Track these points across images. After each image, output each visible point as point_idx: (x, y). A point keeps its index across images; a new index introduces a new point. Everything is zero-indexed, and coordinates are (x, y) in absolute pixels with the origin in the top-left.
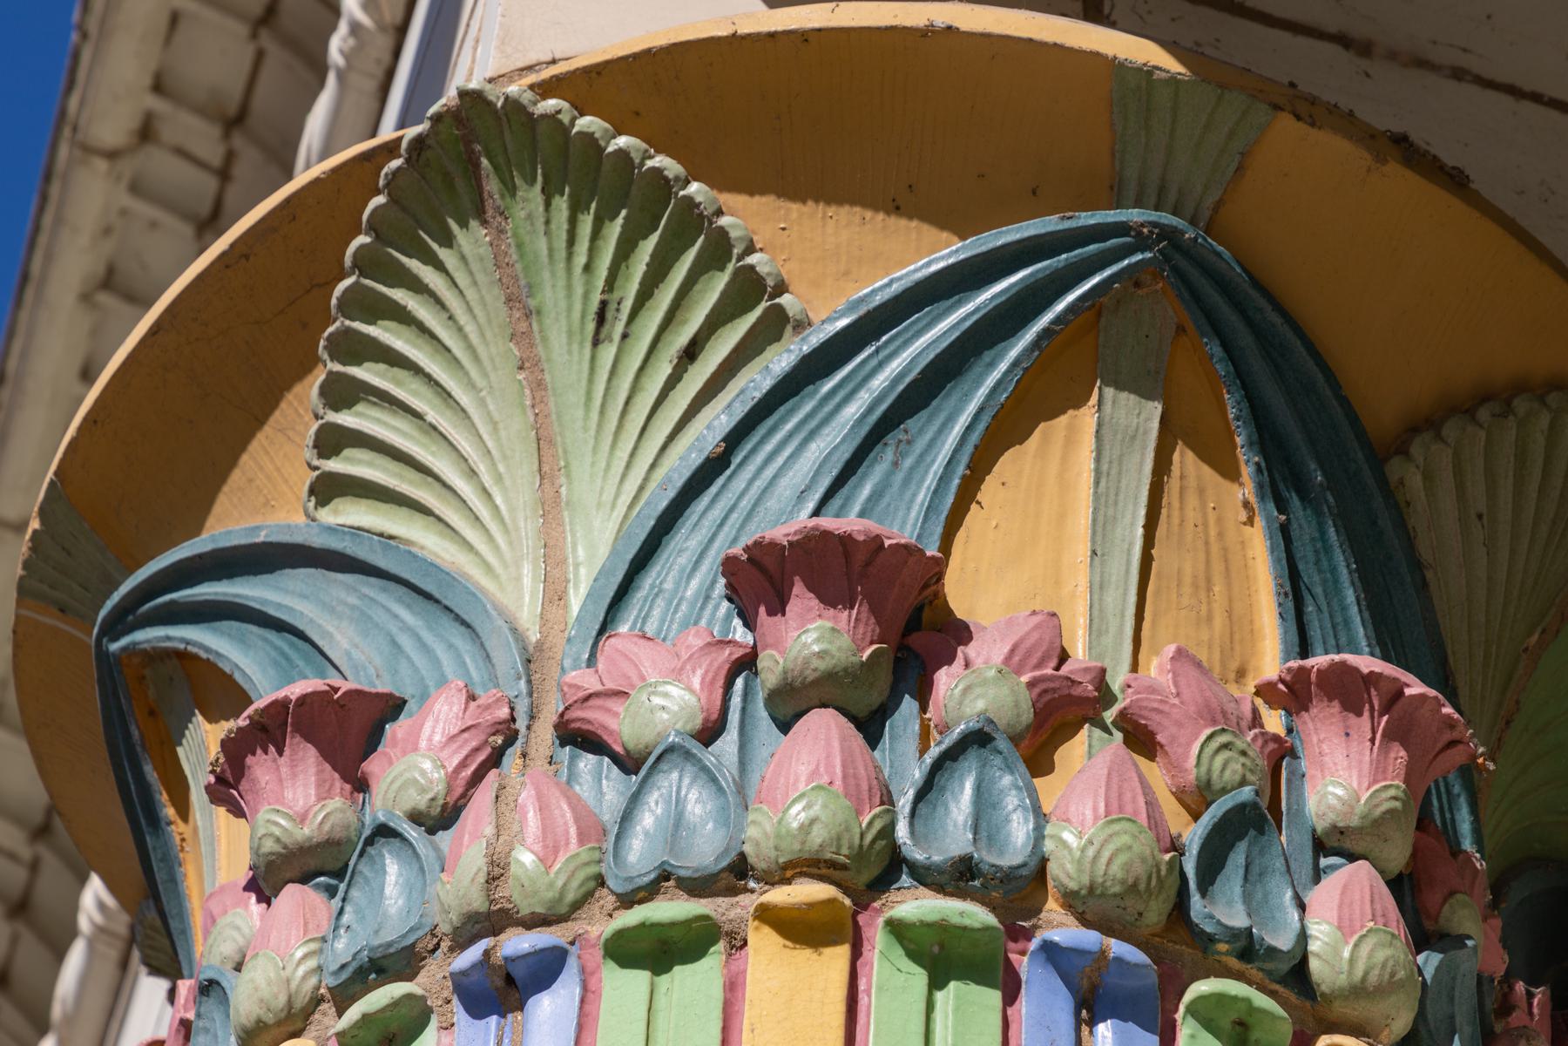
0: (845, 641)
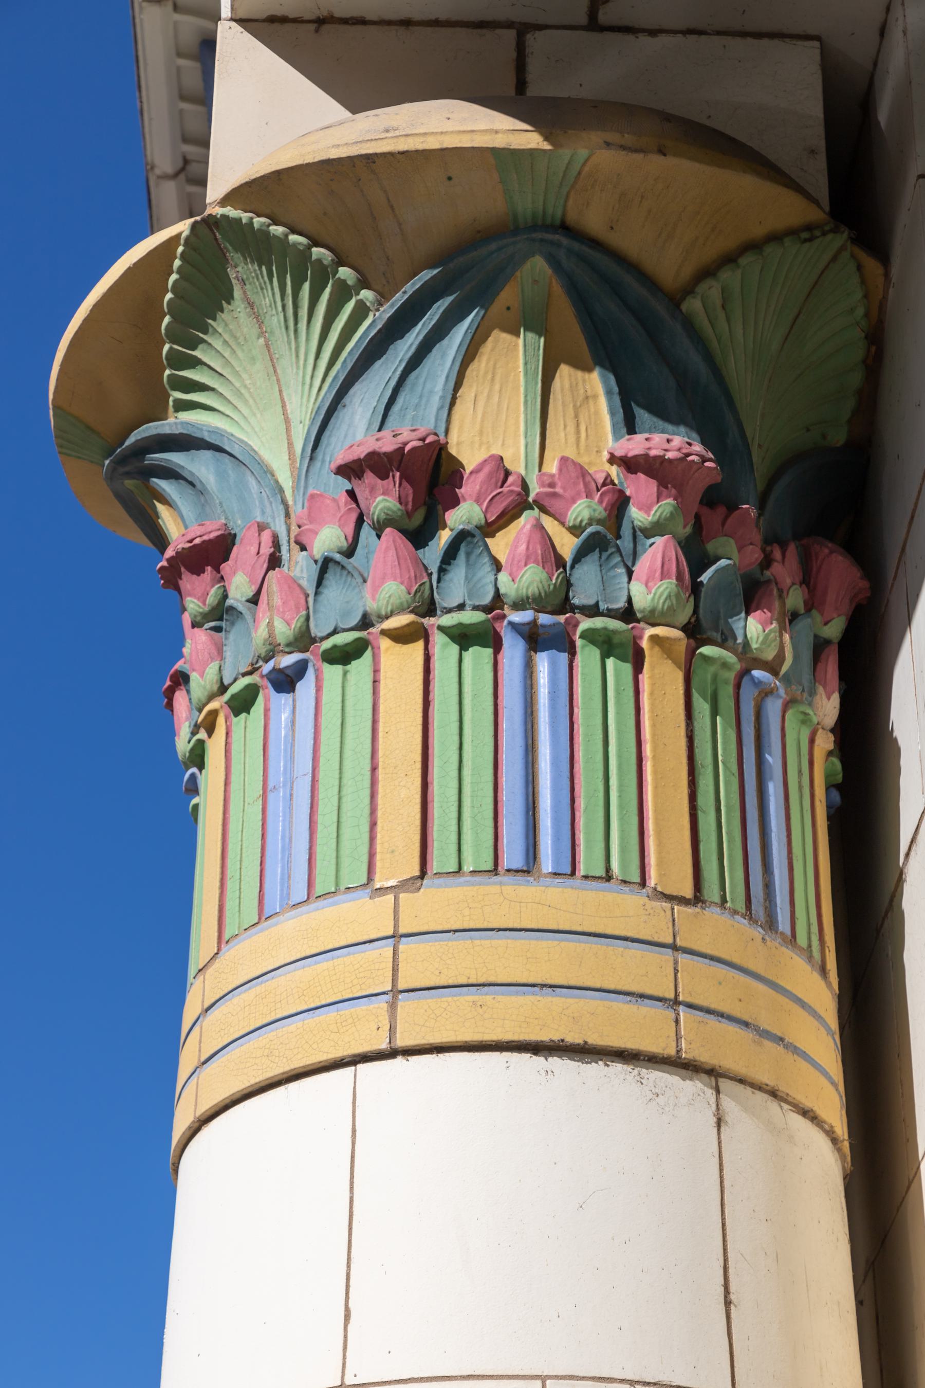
0: (544, 575)
